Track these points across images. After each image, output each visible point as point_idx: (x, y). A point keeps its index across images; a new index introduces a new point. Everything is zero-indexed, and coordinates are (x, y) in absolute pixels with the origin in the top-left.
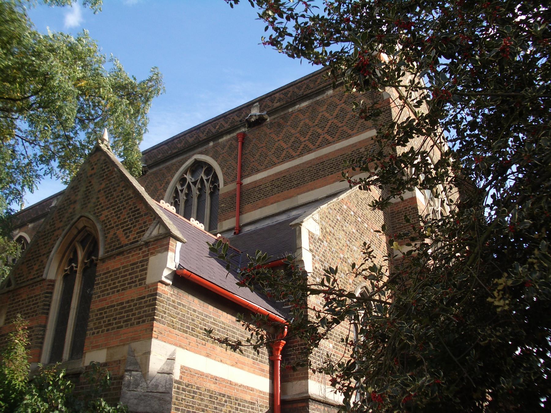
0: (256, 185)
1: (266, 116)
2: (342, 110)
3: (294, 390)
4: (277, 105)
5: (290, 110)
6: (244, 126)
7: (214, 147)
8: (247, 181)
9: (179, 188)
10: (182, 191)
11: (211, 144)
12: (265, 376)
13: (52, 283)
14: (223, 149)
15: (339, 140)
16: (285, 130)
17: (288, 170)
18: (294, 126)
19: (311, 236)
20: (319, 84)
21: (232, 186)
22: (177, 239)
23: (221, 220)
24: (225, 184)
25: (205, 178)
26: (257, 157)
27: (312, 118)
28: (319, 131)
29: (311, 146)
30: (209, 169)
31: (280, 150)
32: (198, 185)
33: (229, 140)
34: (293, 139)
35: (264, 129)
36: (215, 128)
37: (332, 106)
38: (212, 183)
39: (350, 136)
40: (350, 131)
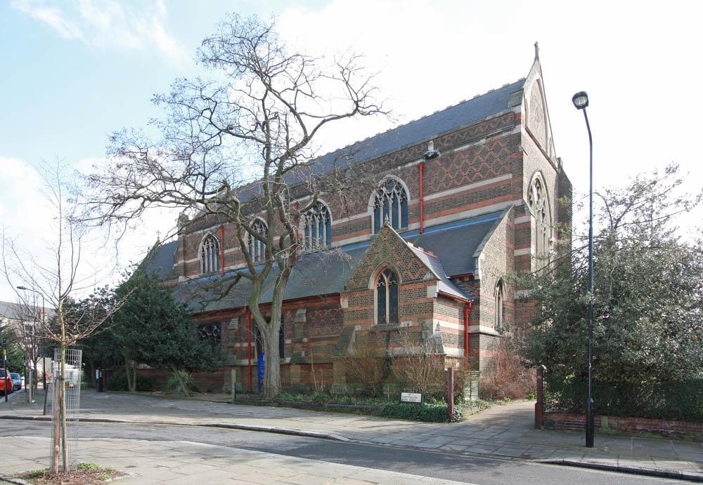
0: (433, 202)
1: (439, 153)
2: (491, 156)
3: (472, 329)
4: (446, 145)
5: (456, 150)
6: (423, 158)
7: (402, 170)
8: (426, 198)
9: (378, 196)
10: (381, 199)
11: (399, 168)
12: (454, 316)
13: (373, 291)
14: (408, 173)
15: (488, 178)
16: (451, 166)
17: (453, 195)
18: (458, 164)
19: (481, 260)
20: (477, 134)
21: (416, 201)
22: (439, 280)
23: (410, 223)
24: (411, 199)
25: (396, 192)
26: (433, 182)
27: (471, 159)
28: (475, 169)
29: (469, 180)
30: (399, 186)
31: (447, 180)
32: (392, 196)
33: (411, 167)
34: (457, 173)
35: (437, 162)
36: (401, 156)
37: (484, 152)
38: (402, 196)
39: (494, 176)
40: (495, 173)
